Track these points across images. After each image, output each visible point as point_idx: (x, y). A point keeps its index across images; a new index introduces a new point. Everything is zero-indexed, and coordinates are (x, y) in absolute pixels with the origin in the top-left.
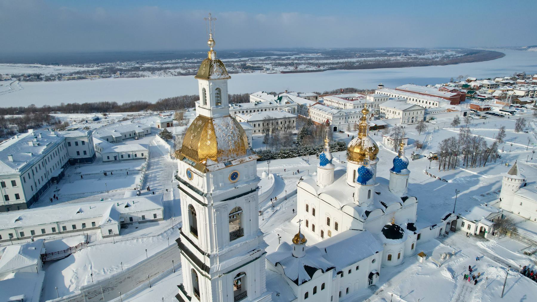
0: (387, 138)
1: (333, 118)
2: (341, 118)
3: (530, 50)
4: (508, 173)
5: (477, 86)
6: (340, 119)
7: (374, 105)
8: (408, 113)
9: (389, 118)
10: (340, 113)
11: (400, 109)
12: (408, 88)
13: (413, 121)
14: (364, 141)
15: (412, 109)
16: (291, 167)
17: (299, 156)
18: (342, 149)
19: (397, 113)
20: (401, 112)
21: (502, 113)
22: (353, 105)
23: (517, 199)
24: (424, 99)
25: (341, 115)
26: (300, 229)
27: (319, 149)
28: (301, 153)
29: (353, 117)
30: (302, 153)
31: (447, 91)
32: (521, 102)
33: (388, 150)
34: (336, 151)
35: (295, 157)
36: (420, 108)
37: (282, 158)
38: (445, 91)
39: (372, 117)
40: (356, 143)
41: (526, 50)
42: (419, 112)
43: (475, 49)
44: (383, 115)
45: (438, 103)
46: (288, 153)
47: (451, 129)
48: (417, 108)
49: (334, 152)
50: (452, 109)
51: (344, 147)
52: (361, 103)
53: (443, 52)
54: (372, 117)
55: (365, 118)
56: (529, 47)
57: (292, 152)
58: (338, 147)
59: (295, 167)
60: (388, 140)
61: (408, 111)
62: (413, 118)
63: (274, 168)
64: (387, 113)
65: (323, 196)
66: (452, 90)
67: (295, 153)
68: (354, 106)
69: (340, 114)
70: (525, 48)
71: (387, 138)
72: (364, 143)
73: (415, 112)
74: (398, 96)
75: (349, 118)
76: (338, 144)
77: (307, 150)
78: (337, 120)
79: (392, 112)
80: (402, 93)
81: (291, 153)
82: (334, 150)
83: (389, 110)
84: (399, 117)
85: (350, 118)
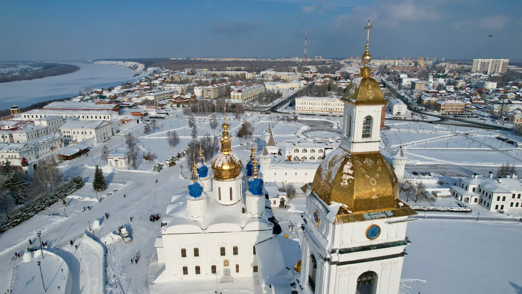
0: (114, 159)
1: (20, 154)
2: (30, 153)
3: (96, 63)
4: (263, 155)
5: (112, 96)
6: (29, 154)
7: (49, 129)
8: (99, 130)
9: (79, 141)
10: (27, 146)
11: (90, 128)
12: (59, 106)
13: (105, 138)
14: (232, 155)
15: (102, 125)
16: (46, 230)
17: (36, 213)
18: (80, 185)
19: (88, 133)
20: (93, 132)
21: (160, 116)
22: (25, 134)
23: (273, 171)
24: (93, 114)
25: (29, 148)
26: (388, 234)
27: (57, 195)
28: (38, 208)
29: (42, 149)
30: (40, 208)
31: (105, 103)
32: (160, 105)
33: (123, 170)
34: (76, 190)
35: (32, 216)
36: (108, 123)
37: (14, 226)
38: (103, 103)
39: (62, 143)
40: (227, 160)
41: (93, 63)
42: (107, 127)
43: (48, 62)
44: (69, 138)
45: (109, 116)
46: (20, 216)
47: (145, 136)
48: (105, 123)
49: (74, 191)
50: (125, 119)
51: (81, 183)
52: (34, 130)
53: (14, 66)
54: (62, 143)
55: (227, 133)
56: (95, 61)
57: (25, 212)
58: (75, 185)
59: (51, 227)
60: (115, 161)
61: (99, 128)
62: (104, 134)
63: (22, 243)
64: (74, 136)
65: (212, 228)
66: (109, 102)
67: (30, 212)
68: (28, 135)
69: (28, 148)
70: (91, 61)
71: (114, 159)
72: (234, 158)
73: (105, 128)
74: (45, 116)
75: (38, 151)
76: (75, 181)
77: (44, 202)
78: (27, 156)
79: (80, 133)
80: (61, 112)
81: (24, 214)
82: (73, 191)
83: (76, 131)
84: (91, 136)
85: (40, 149)
